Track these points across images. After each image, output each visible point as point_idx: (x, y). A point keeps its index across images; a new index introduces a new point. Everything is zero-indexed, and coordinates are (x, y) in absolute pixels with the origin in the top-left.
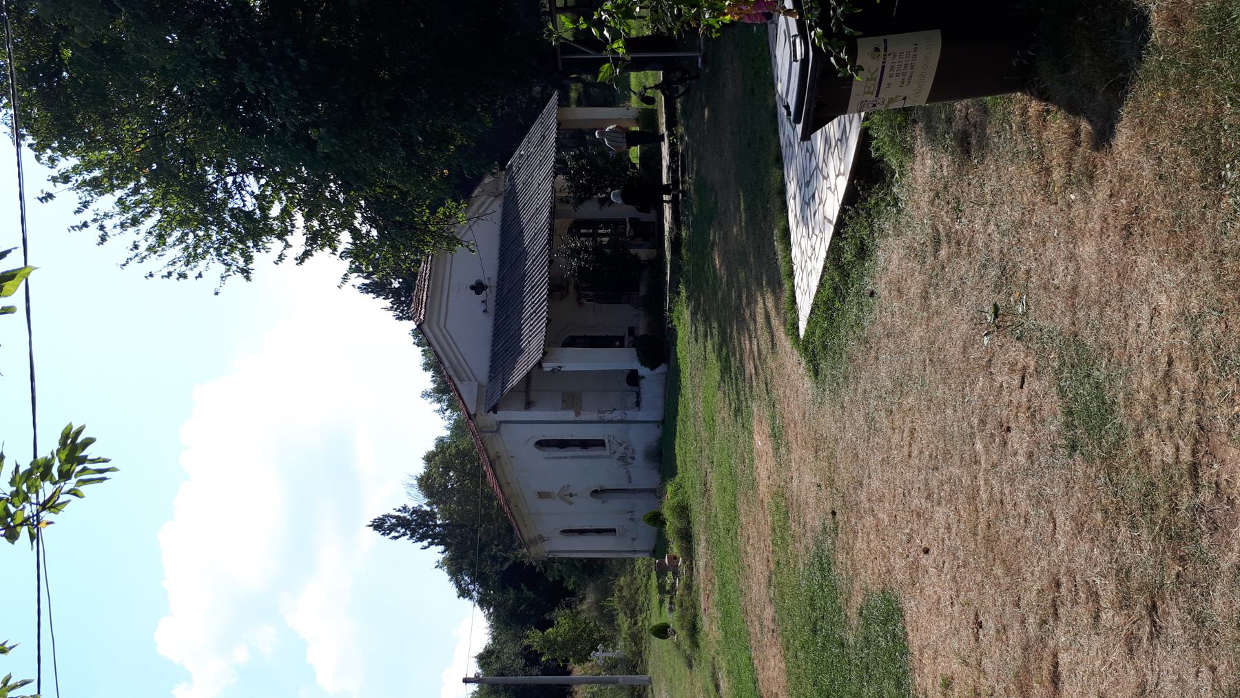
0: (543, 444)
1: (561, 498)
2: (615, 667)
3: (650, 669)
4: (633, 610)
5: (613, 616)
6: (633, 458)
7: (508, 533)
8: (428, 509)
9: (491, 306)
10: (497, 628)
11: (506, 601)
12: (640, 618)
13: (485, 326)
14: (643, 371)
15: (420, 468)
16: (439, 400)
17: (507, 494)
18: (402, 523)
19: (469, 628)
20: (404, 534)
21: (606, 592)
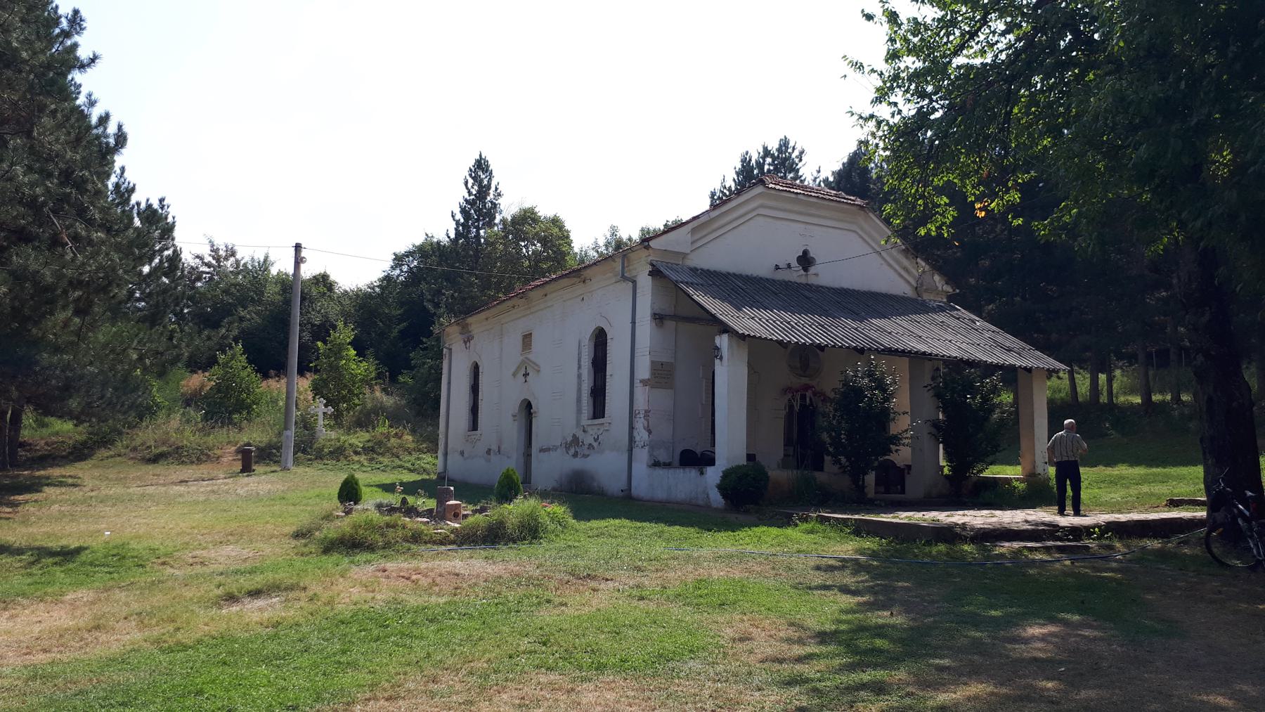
0: (600, 339)
1: (523, 362)
2: (305, 427)
3: (300, 470)
4: (373, 450)
5: (367, 426)
6: (575, 455)
7: (466, 308)
8: (497, 221)
9: (780, 276)
10: (357, 295)
11: (389, 306)
12: (363, 458)
13: (760, 267)
14: (713, 475)
15: (545, 211)
16: (607, 245)
17: (532, 294)
18: (483, 191)
19: (358, 267)
20: (470, 193)
21: (395, 418)
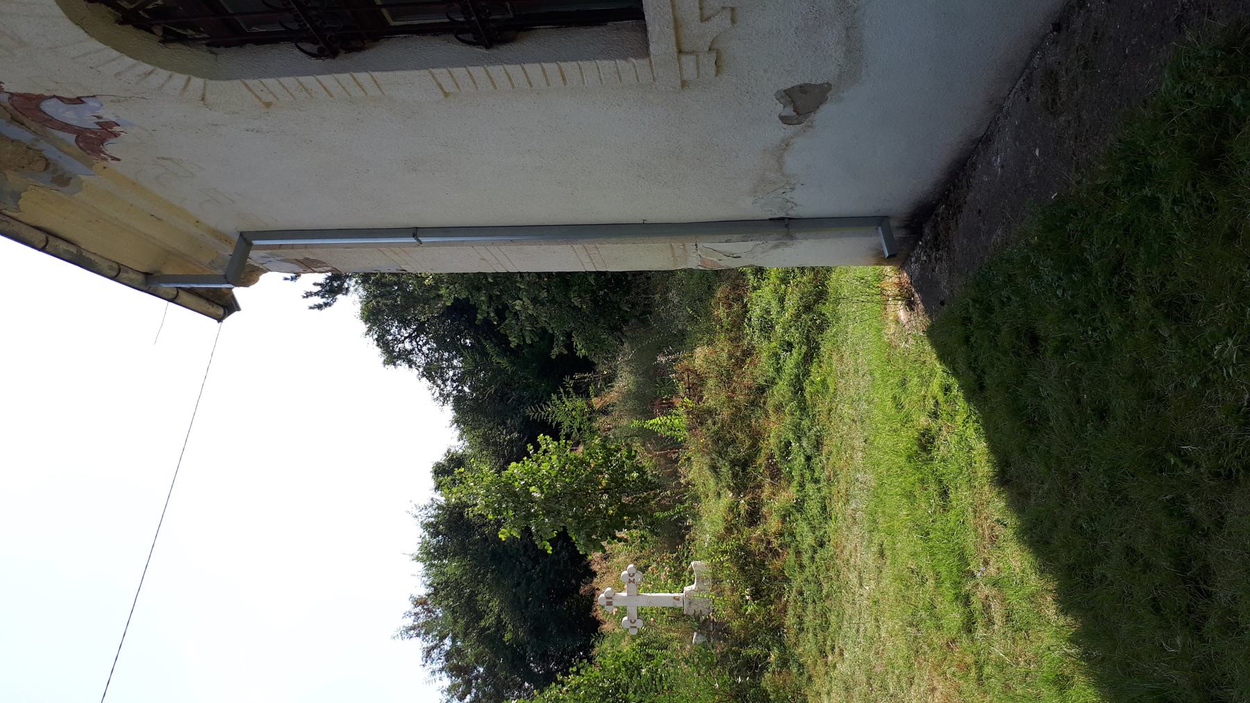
4: (743, 465)
12: (777, 501)
